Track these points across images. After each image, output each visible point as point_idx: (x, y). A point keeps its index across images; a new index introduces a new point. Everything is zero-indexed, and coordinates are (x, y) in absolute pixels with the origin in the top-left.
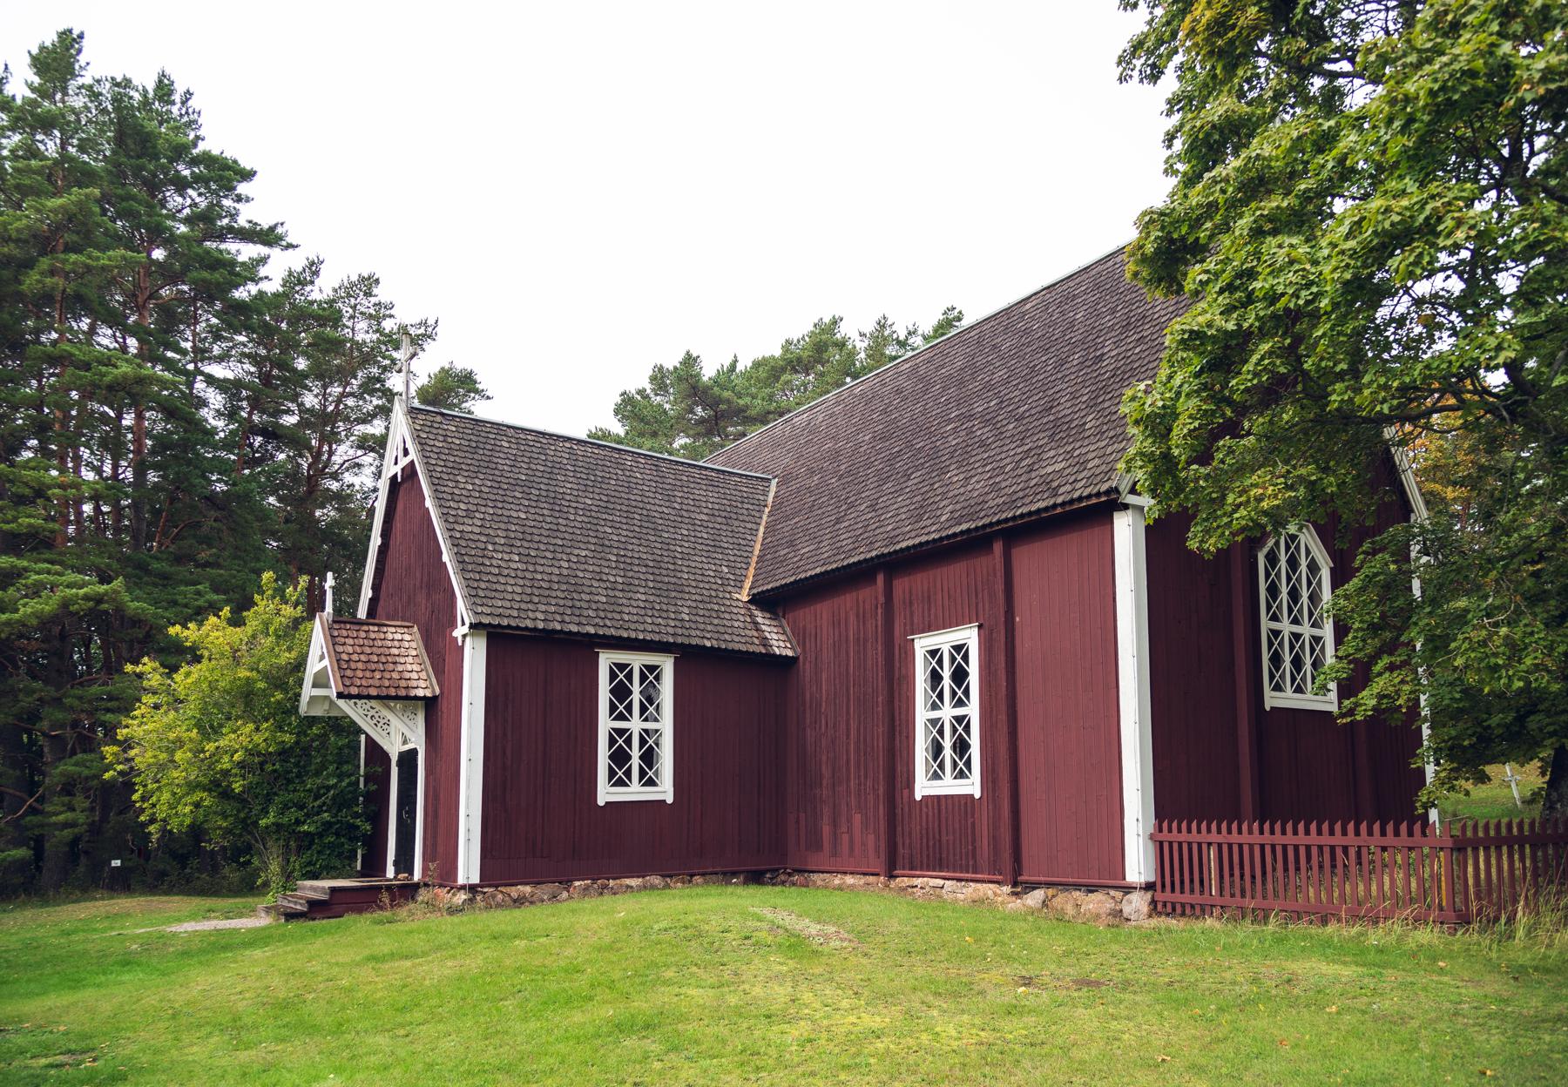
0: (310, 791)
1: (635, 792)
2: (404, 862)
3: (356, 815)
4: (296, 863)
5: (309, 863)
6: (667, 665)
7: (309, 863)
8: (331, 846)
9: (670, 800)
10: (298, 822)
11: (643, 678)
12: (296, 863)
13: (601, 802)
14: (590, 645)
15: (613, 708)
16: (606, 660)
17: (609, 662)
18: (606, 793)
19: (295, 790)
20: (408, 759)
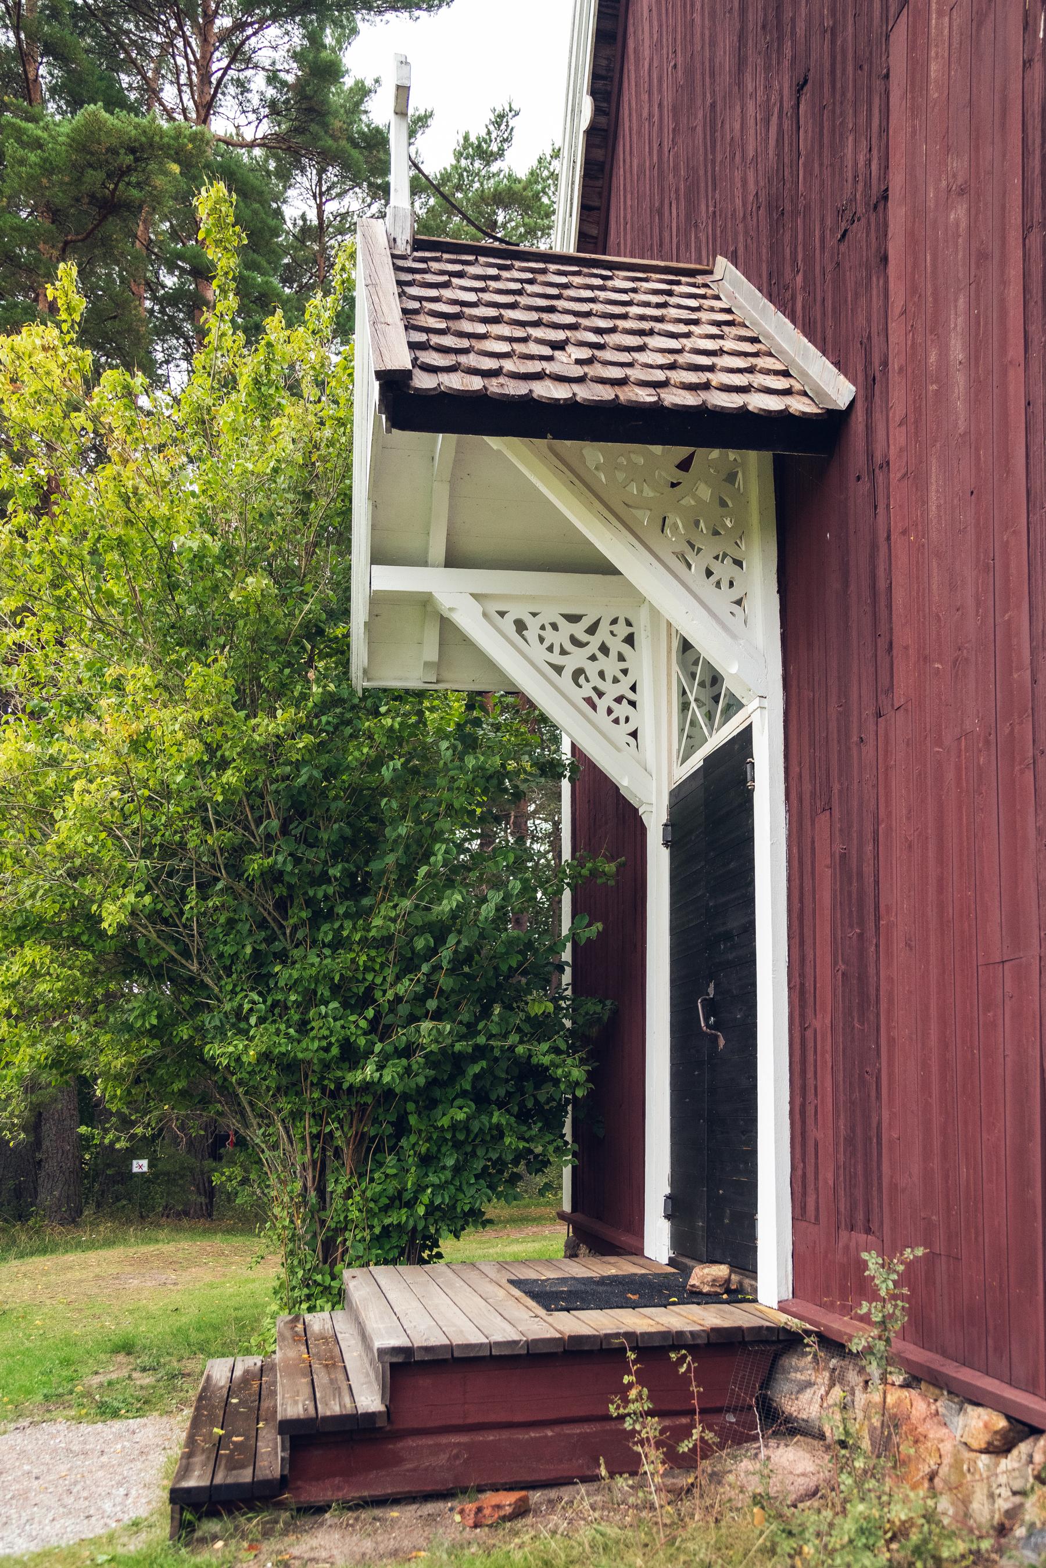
0: (386, 942)
2: (715, 1213)
3: (541, 1028)
4: (350, 1198)
5: (399, 1200)
7: (399, 1200)
8: (462, 1139)
10: (351, 1055)
12: (350, 1198)
19: (338, 944)
20: (714, 805)
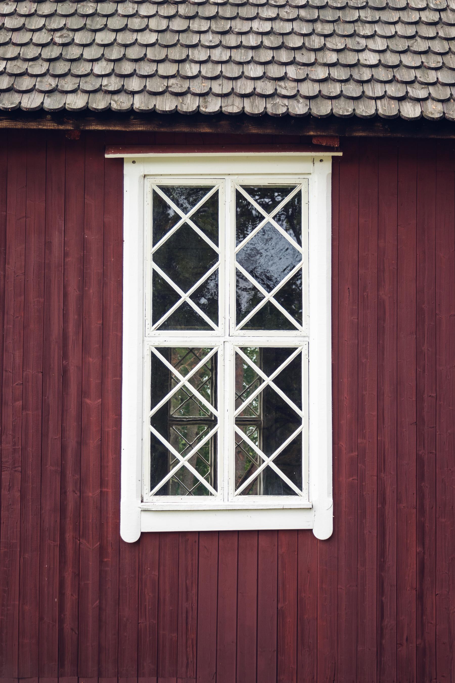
1: (226, 508)
6: (313, 180)
9: (323, 530)
11: (246, 219)
13: (129, 533)
14: (79, 148)
15: (162, 298)
16: (143, 179)
17: (151, 185)
18: (141, 511)
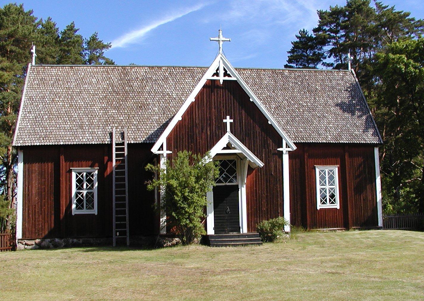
13: (318, 208)
